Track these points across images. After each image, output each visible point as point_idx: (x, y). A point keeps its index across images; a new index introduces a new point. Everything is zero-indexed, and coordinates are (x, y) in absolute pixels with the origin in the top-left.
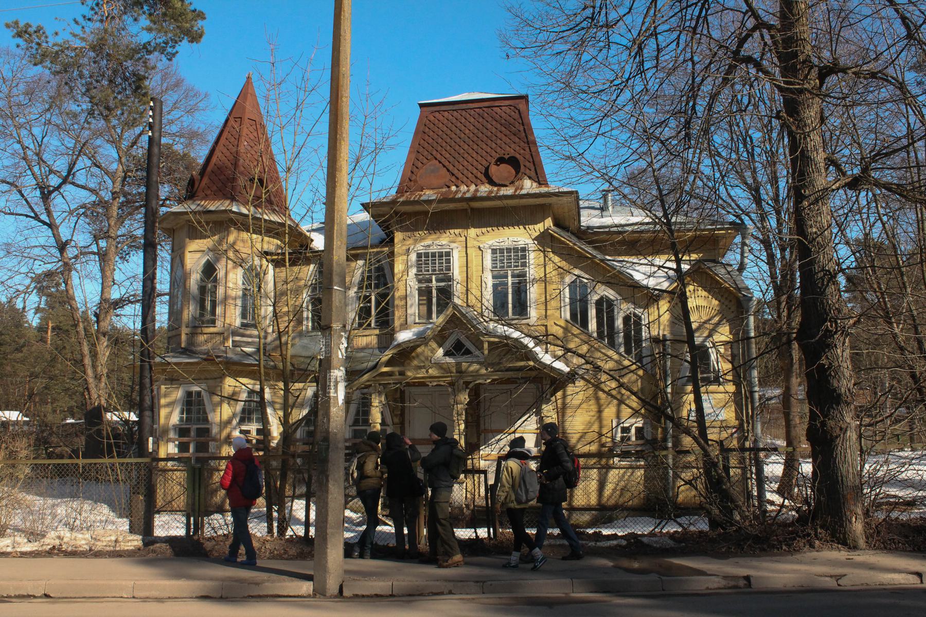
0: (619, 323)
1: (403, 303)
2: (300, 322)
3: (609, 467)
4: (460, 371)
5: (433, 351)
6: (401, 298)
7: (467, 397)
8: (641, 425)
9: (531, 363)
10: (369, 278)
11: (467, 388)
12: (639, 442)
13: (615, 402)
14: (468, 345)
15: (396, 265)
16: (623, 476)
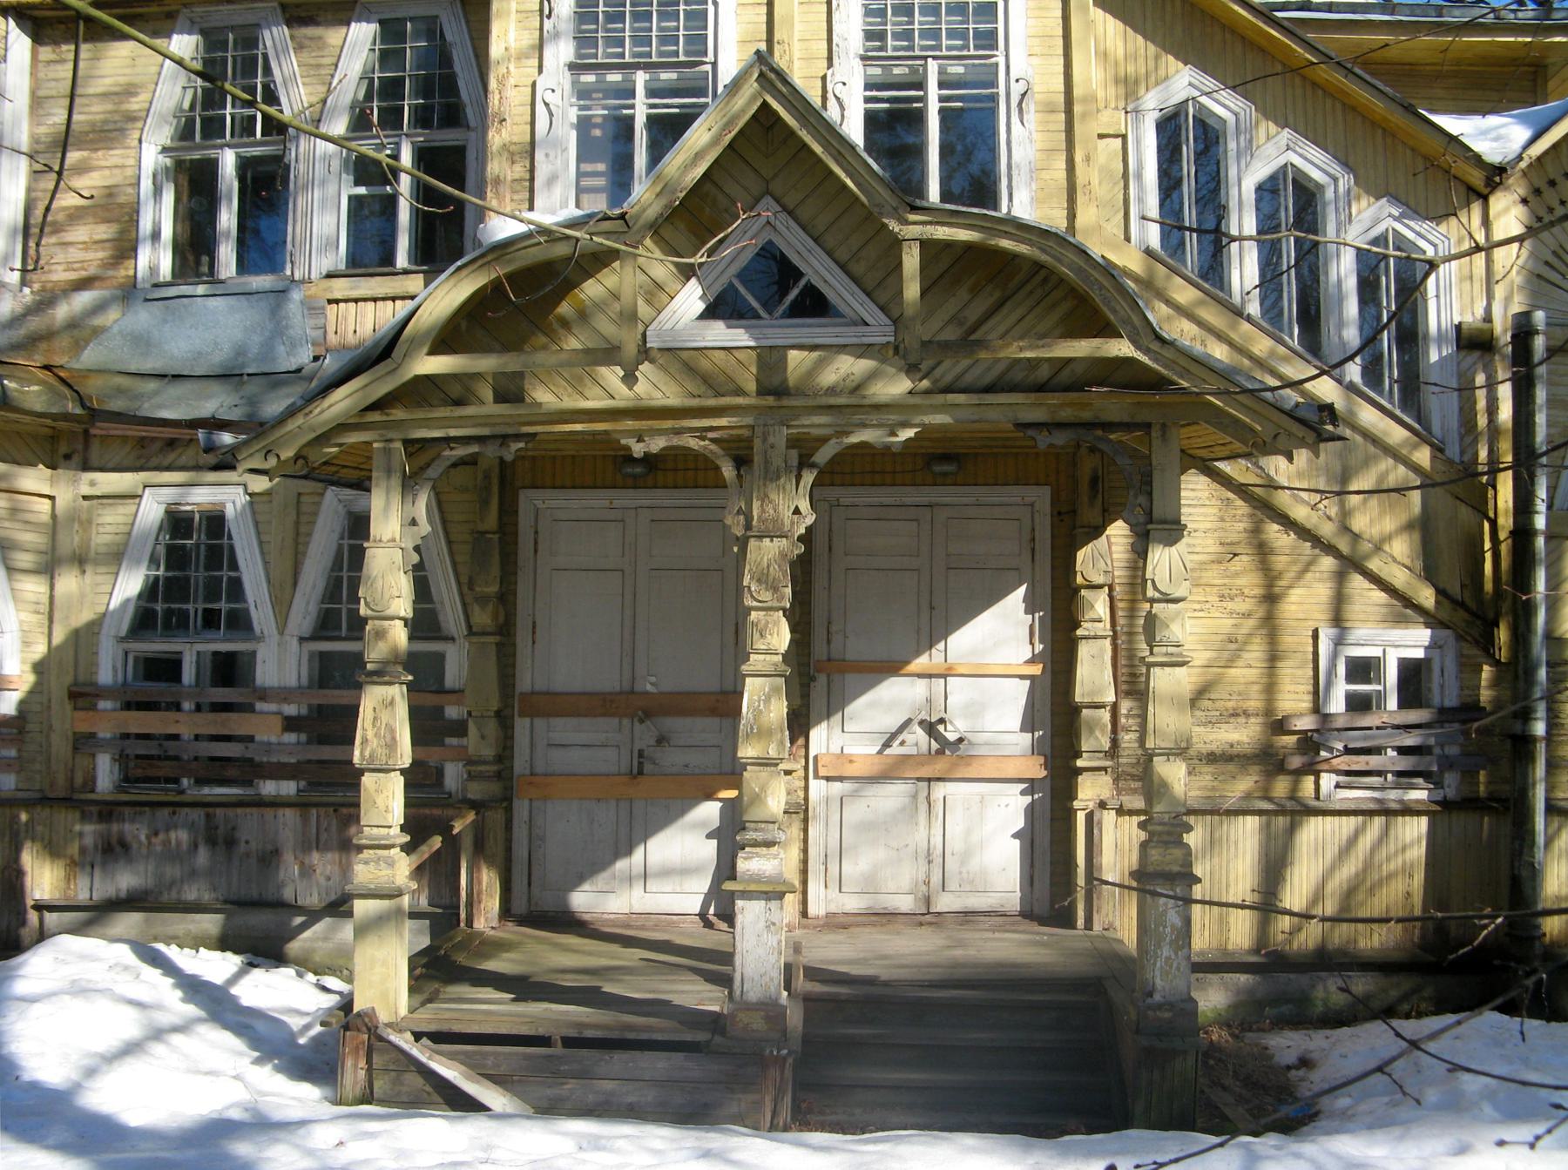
0: (1343, 271)
1: (519, 170)
2: (125, 248)
3: (1301, 811)
4: (774, 386)
5: (657, 294)
6: (510, 152)
7: (804, 505)
8: (1419, 654)
9: (1122, 348)
10: (392, 89)
11: (804, 462)
12: (1414, 716)
13: (1328, 563)
14: (818, 269)
15: (496, 29)
16: (1353, 841)
